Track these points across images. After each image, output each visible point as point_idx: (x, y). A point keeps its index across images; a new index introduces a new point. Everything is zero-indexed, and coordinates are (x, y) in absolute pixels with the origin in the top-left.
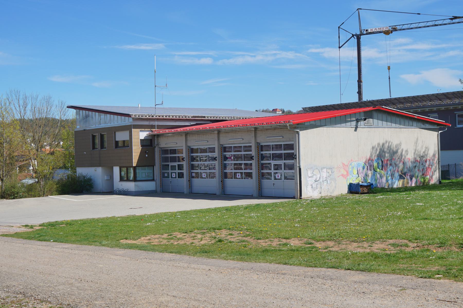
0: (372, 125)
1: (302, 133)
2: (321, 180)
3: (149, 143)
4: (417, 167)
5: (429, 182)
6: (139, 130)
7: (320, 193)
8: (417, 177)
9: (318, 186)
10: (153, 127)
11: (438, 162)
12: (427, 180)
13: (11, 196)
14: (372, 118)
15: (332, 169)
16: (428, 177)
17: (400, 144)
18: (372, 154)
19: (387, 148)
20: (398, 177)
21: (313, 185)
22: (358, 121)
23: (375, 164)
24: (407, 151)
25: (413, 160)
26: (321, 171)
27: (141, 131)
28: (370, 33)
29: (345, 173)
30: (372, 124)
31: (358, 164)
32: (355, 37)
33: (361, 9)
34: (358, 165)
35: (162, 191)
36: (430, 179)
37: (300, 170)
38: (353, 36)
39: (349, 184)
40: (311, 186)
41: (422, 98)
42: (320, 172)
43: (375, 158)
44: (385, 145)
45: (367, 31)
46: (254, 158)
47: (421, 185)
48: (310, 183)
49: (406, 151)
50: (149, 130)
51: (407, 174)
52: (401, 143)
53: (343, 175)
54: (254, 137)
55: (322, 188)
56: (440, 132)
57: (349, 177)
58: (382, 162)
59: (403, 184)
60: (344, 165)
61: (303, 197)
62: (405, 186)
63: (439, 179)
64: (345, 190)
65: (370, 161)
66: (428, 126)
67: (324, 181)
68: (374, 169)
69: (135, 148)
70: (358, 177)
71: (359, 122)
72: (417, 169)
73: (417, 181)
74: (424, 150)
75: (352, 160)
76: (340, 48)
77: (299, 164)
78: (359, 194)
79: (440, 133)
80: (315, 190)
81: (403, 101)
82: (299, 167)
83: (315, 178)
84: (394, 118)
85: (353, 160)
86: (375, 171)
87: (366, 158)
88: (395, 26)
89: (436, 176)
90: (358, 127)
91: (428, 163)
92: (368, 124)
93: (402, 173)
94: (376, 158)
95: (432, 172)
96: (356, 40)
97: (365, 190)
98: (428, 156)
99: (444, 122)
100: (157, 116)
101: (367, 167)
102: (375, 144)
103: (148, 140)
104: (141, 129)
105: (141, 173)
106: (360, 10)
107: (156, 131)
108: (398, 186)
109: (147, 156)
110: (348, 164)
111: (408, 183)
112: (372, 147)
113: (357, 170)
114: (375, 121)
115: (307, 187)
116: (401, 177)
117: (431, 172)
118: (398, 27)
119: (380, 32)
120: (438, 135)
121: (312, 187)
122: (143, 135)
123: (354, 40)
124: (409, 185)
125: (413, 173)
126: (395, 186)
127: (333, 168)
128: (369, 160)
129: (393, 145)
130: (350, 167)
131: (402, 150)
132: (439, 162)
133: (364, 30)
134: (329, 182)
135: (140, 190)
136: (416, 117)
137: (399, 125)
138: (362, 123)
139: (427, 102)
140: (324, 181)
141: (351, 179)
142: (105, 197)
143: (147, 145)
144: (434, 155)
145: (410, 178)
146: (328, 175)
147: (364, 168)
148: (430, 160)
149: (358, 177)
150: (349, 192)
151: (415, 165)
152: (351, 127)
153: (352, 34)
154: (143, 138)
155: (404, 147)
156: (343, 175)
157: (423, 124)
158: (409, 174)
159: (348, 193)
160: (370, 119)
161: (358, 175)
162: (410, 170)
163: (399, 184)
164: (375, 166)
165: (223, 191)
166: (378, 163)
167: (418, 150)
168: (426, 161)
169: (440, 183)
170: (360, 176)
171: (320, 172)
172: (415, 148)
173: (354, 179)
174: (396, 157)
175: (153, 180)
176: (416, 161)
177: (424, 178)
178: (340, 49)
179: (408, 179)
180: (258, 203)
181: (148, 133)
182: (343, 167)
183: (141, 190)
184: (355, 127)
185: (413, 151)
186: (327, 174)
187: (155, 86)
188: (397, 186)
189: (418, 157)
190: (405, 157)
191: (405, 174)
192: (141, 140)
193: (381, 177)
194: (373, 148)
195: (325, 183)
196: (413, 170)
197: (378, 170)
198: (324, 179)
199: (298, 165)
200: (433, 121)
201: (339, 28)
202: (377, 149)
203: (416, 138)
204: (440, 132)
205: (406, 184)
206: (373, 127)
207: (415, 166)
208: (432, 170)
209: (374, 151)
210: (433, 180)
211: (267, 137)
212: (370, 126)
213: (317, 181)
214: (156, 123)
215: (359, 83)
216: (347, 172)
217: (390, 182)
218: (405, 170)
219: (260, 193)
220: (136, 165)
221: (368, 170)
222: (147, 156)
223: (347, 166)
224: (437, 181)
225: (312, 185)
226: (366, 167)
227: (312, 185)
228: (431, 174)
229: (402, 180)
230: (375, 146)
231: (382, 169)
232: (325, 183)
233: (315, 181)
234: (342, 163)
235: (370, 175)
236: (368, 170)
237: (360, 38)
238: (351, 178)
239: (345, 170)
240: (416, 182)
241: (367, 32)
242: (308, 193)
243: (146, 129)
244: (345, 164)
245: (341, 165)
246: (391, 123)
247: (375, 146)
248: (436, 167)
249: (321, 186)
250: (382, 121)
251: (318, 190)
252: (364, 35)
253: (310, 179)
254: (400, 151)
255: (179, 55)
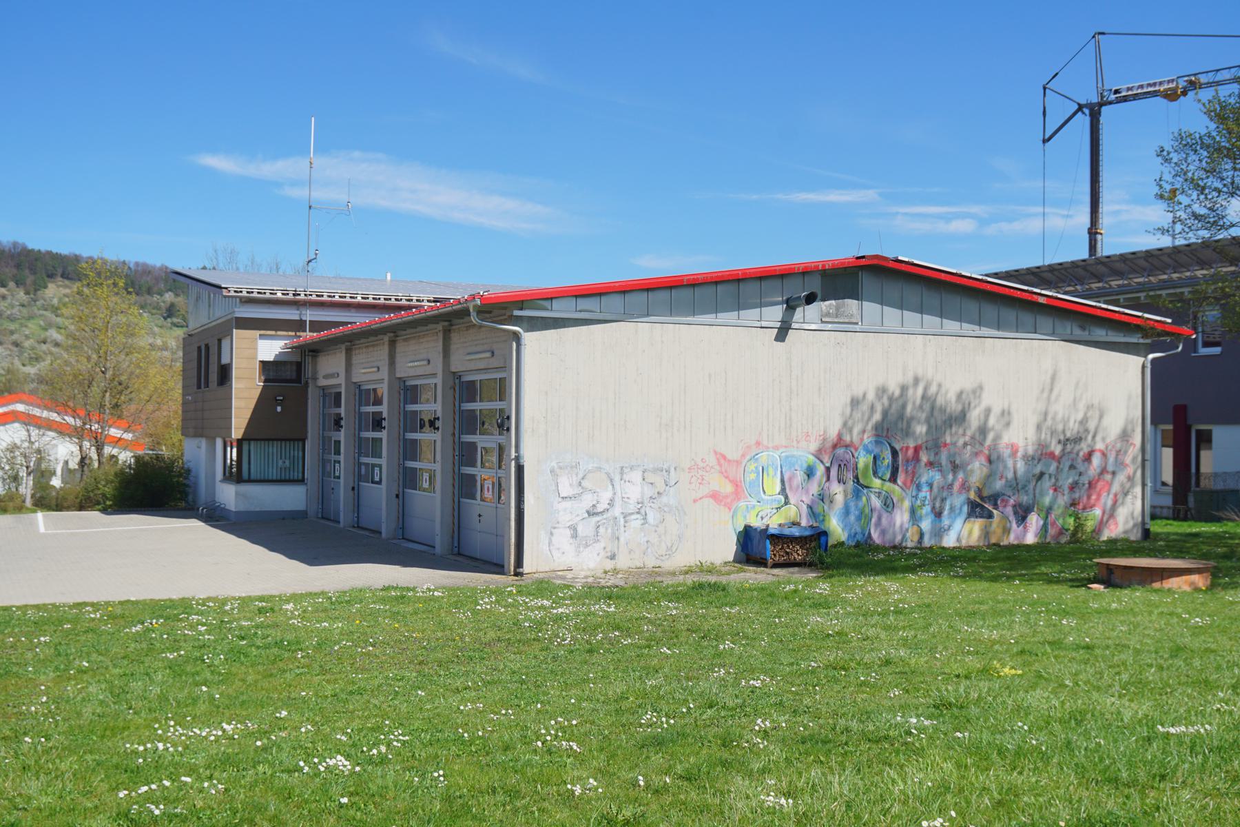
0: (857, 324)
1: (531, 340)
2: (617, 511)
3: (294, 374)
4: (1047, 476)
5: (1098, 530)
6: (258, 333)
7: (613, 557)
8: (1049, 510)
9: (602, 530)
10: (299, 325)
11: (1140, 458)
12: (1090, 525)
13: (98, 503)
14: (855, 295)
15: (668, 471)
16: (1097, 512)
17: (978, 390)
18: (850, 423)
19: (918, 402)
20: (965, 509)
21: (580, 529)
22: (791, 306)
23: (863, 460)
24: (1006, 414)
25: (1030, 451)
26: (617, 478)
27: (262, 337)
28: (1125, 99)
29: (728, 488)
30: (857, 319)
31: (787, 457)
32: (1087, 111)
33: (1103, 34)
34: (787, 461)
35: (320, 516)
36: (1105, 519)
37: (520, 470)
38: (1080, 108)
39: (741, 528)
40: (568, 532)
41: (1173, 256)
42: (611, 480)
43: (861, 435)
44: (910, 392)
45: (1117, 92)
46: (384, 424)
47: (1064, 540)
48: (565, 519)
49: (1003, 413)
50: (290, 333)
51: (1005, 502)
52: (981, 388)
53: (715, 496)
54: (441, 355)
55: (622, 539)
56: (1151, 356)
57: (742, 504)
58: (895, 453)
59: (986, 533)
60: (722, 462)
61: (527, 567)
62: (993, 541)
63: (1143, 523)
64: (727, 549)
65: (840, 451)
66: (1100, 334)
67: (633, 513)
68: (856, 477)
69: (241, 386)
70: (786, 503)
71: (799, 310)
72: (1047, 483)
73: (1045, 525)
74: (1080, 416)
75: (758, 443)
76: (1045, 141)
77: (517, 449)
78: (765, 565)
79: (1154, 360)
80: (587, 546)
81: (1120, 266)
82: (517, 458)
83: (587, 501)
84: (954, 301)
85: (765, 443)
86: (860, 486)
87: (824, 440)
88: (1195, 75)
89: (1131, 510)
90: (794, 326)
91: (1096, 460)
92: (837, 317)
93: (982, 498)
94: (868, 439)
95: (1116, 495)
96: (1087, 119)
97: (798, 554)
98: (1098, 438)
99: (1169, 321)
100: (311, 295)
101: (828, 470)
102: (867, 386)
103: (291, 363)
104: (262, 332)
105: (262, 458)
106: (1100, 36)
107: (308, 335)
108: (964, 543)
109: (279, 409)
110: (743, 456)
111: (1007, 531)
112: (849, 400)
113: (783, 481)
114: (871, 308)
115: (552, 534)
116: (977, 509)
117: (1111, 496)
118: (1203, 79)
119: (1154, 94)
120: (1144, 367)
121: (575, 535)
122: (270, 348)
123: (1083, 121)
124: (1012, 539)
125: (1031, 496)
126: (949, 541)
127: (672, 470)
128: (835, 446)
129: (946, 393)
130: (752, 467)
131: (988, 411)
132: (1144, 460)
133: (1111, 90)
134: (650, 518)
135: (252, 509)
136: (1042, 300)
137: (977, 327)
138: (809, 314)
139: (1191, 268)
140: (633, 513)
141: (754, 513)
142: (157, 524)
143: (289, 378)
144: (1125, 436)
145: (1015, 513)
146: (649, 492)
147: (810, 473)
148: (1104, 454)
149: (786, 503)
150: (743, 556)
151: (1038, 470)
152: (758, 324)
153: (1079, 104)
154: (270, 357)
155: (992, 399)
156: (715, 496)
157: (1083, 328)
158: (1012, 501)
159: (737, 560)
160: (849, 301)
161: (786, 497)
162: (1016, 485)
163: (970, 533)
164: (861, 465)
165: (401, 526)
166: (875, 458)
167: (1056, 413)
168: (1088, 457)
169: (1146, 533)
170: (792, 500)
171: (611, 480)
172: (1041, 407)
173: (767, 510)
174: (956, 437)
175: (302, 481)
176: (1042, 454)
177: (1077, 518)
178: (1047, 144)
179: (1005, 518)
180: (347, 586)
181: (281, 343)
182: (718, 468)
183: (258, 509)
184: (778, 325)
185: (1033, 420)
186: (646, 488)
187: (310, 207)
188: (958, 540)
189: (1054, 442)
190: (998, 437)
191: (995, 499)
192: (262, 362)
193: (889, 504)
194: (855, 403)
195: (636, 522)
196: (1031, 486)
197: (877, 483)
198: (632, 507)
199: (513, 455)
200: (1116, 317)
201: (1045, 88)
202: (872, 408)
203: (1050, 373)
204: (1151, 356)
205: (999, 531)
206: (857, 328)
207: (1042, 474)
208: (1116, 488)
209: (857, 415)
210: (1116, 524)
211: (469, 354)
212: (848, 326)
213: (597, 514)
214: (309, 315)
215: (1093, 236)
216: (737, 485)
217: (926, 525)
218: (999, 485)
219: (456, 544)
220: (245, 433)
221: (828, 479)
222: (279, 409)
223: (738, 463)
224: (1135, 525)
225: (574, 529)
226: (820, 470)
227: (574, 529)
228: (1110, 503)
229: (980, 520)
230: (864, 395)
231: (893, 479)
232: (636, 522)
233: (591, 513)
234: (715, 452)
235: (839, 498)
236: (828, 479)
237: (1099, 113)
238: (754, 507)
239: (727, 477)
240: (1045, 528)
241: (1118, 95)
242: (556, 554)
243: (279, 333)
244: (729, 457)
245: (712, 460)
246: (941, 317)
247: (864, 395)
248: (1130, 479)
249: (613, 533)
250: (922, 313)
251: (602, 545)
252: (1111, 103)
253: (567, 504)
254: (975, 417)
255: (906, 214)
